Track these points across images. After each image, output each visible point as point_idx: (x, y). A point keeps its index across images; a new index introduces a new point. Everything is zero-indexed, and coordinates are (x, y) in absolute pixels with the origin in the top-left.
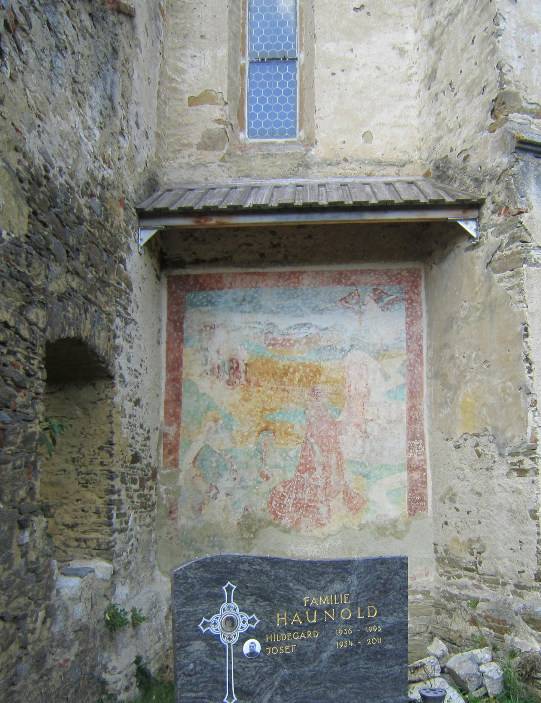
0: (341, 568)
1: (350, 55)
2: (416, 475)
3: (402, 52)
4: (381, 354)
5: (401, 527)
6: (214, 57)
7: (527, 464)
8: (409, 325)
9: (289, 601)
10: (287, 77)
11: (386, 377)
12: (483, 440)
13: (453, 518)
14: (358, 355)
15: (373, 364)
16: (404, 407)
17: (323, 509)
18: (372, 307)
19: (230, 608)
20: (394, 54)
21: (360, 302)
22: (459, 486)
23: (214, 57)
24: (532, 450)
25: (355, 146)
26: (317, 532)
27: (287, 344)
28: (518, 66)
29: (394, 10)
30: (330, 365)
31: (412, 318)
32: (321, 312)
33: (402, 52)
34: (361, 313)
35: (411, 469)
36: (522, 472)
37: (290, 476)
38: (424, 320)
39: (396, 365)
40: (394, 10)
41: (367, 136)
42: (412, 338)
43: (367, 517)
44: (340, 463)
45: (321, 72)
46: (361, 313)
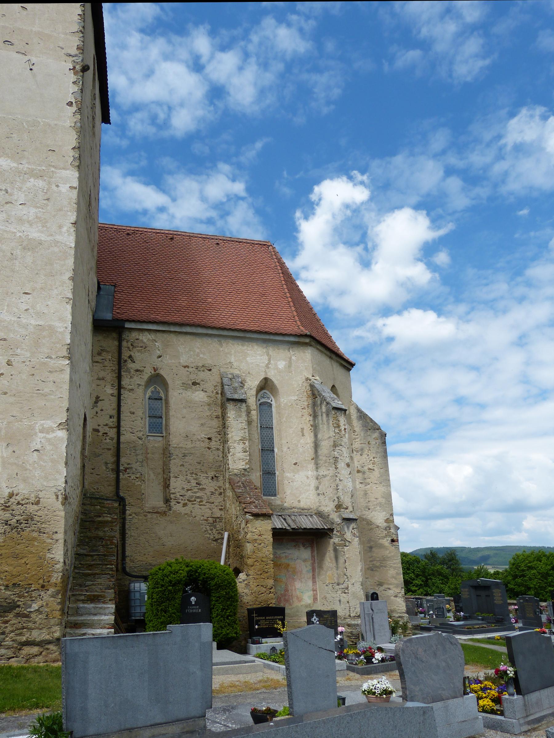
0: (328, 612)
1: (294, 478)
2: (315, 592)
3: (308, 478)
4: (305, 561)
5: (311, 605)
6: (256, 476)
7: (346, 591)
8: (312, 553)
9: (322, 617)
10: (273, 478)
11: (306, 567)
12: (334, 585)
13: (325, 603)
14: (299, 561)
15: (303, 563)
16: (311, 574)
17: (291, 601)
18: (302, 548)
19: (315, 617)
20: (305, 478)
21: (299, 547)
22: (328, 596)
23: (256, 476)
24: (348, 588)
25: (296, 504)
26: (290, 607)
27: (280, 558)
28: (342, 497)
29: (305, 465)
30: (292, 563)
31: (312, 552)
32: (289, 549)
33: (308, 478)
34: (299, 550)
35: (313, 591)
36: (345, 593)
37: (282, 593)
38: (316, 552)
39: (309, 563)
40: (305, 465)
41: (299, 501)
42: (313, 557)
43: (303, 603)
44: (295, 589)
45: (286, 482)
46: (299, 550)
